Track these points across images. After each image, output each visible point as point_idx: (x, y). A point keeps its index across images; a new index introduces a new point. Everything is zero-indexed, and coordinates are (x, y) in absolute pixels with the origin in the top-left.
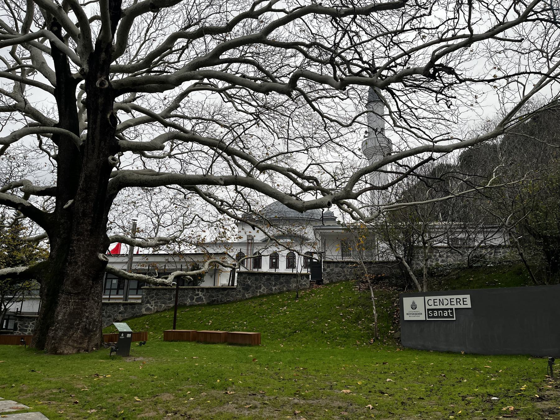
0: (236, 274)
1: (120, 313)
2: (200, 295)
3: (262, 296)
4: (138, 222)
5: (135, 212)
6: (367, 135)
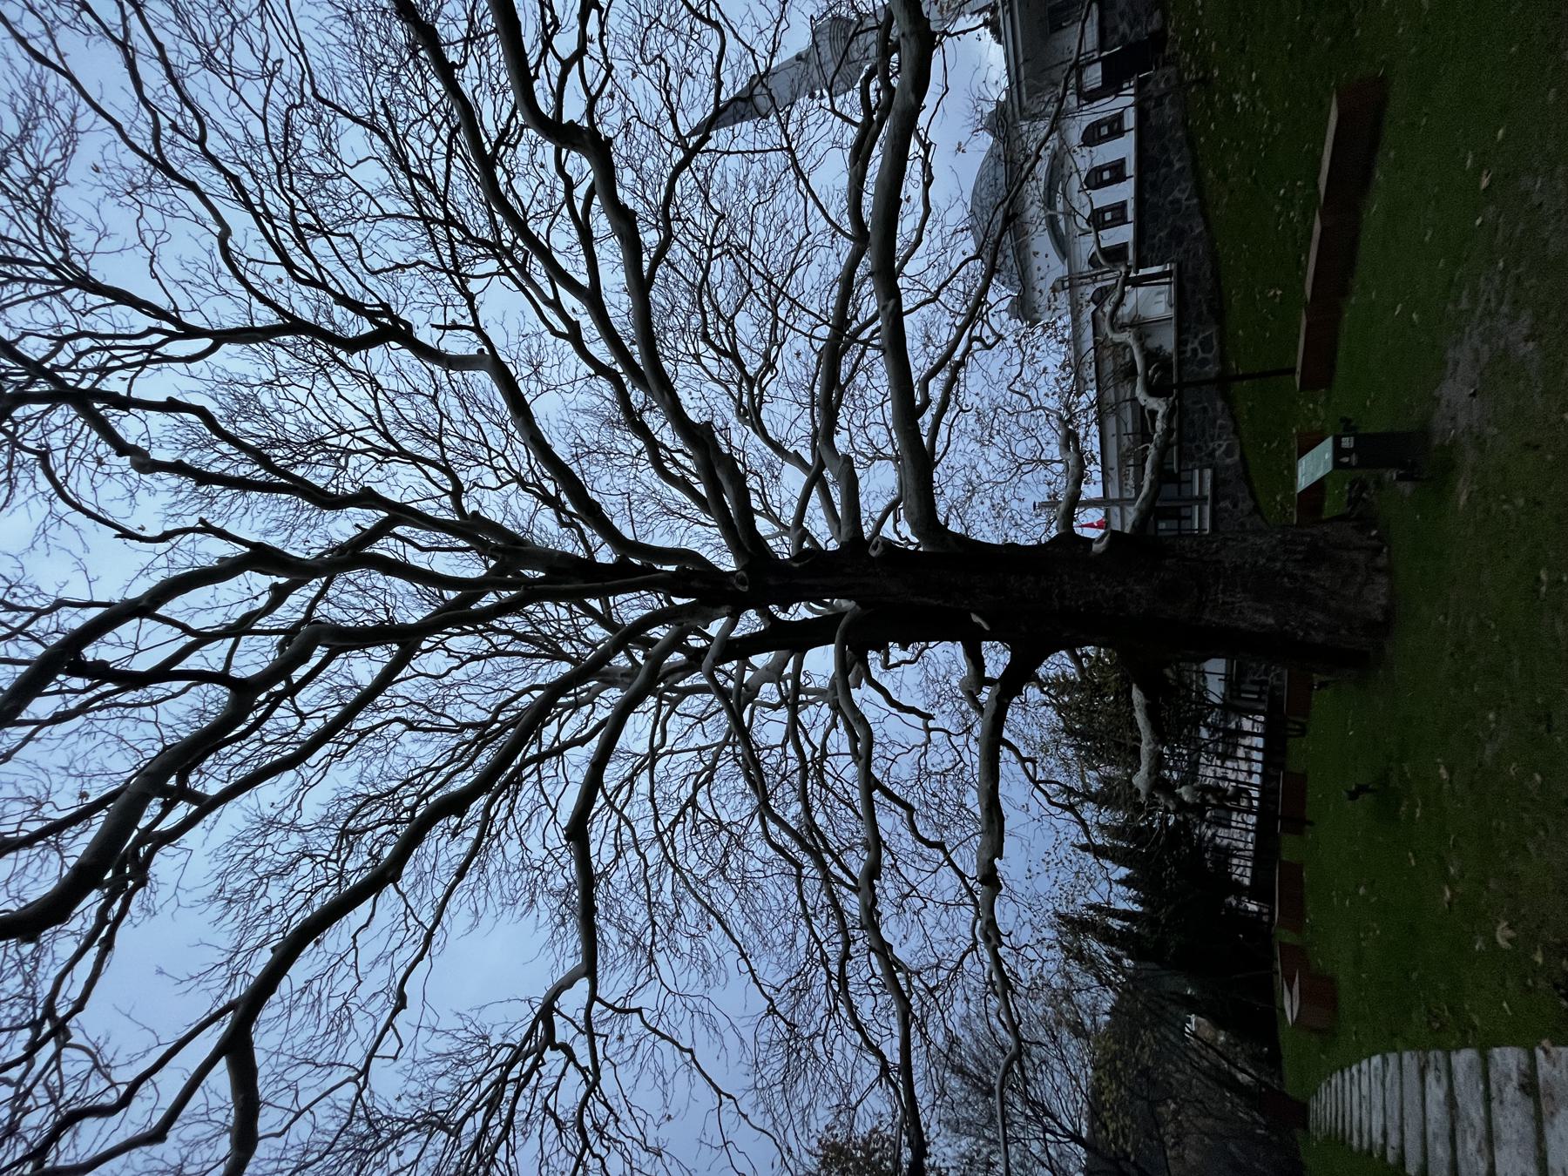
0: (1142, 272)
1: (1235, 506)
2: (1196, 344)
3: (1199, 190)
4: (1038, 501)
5: (1015, 504)
6: (818, 93)
